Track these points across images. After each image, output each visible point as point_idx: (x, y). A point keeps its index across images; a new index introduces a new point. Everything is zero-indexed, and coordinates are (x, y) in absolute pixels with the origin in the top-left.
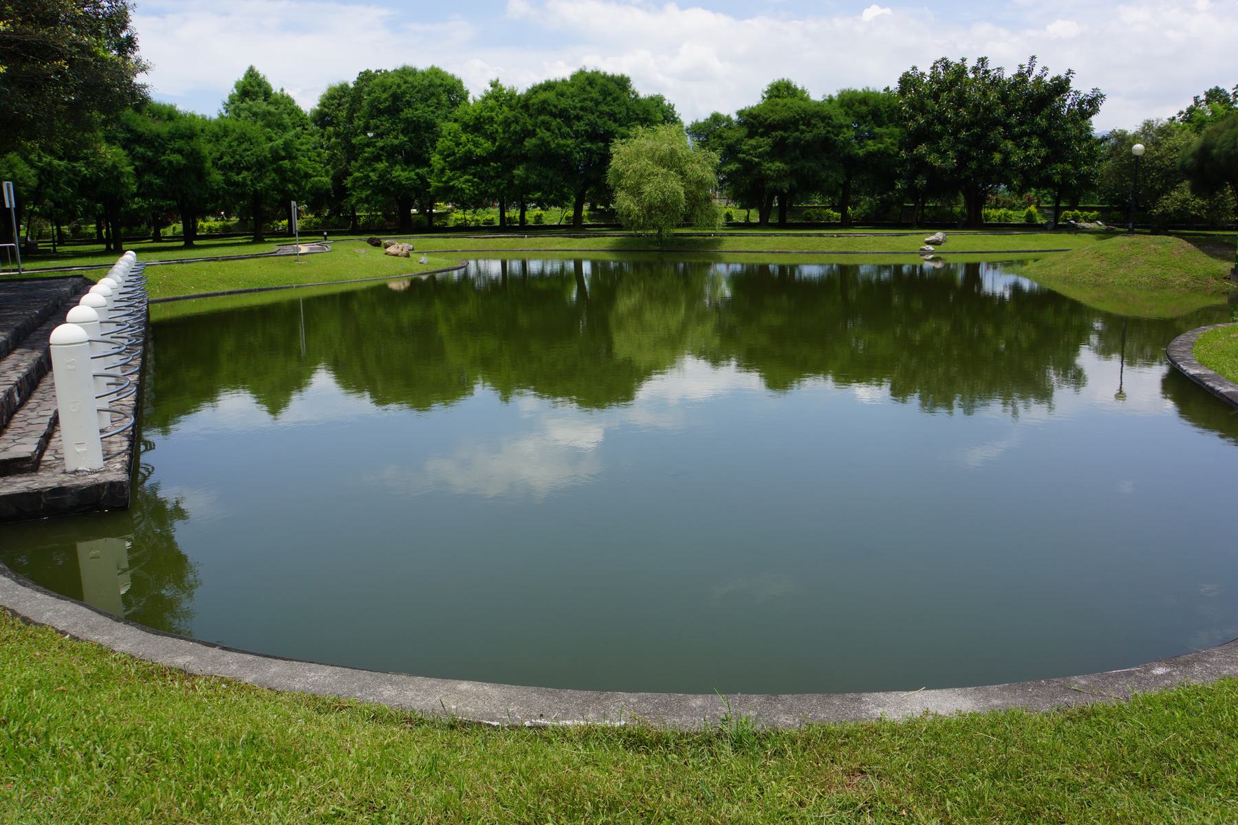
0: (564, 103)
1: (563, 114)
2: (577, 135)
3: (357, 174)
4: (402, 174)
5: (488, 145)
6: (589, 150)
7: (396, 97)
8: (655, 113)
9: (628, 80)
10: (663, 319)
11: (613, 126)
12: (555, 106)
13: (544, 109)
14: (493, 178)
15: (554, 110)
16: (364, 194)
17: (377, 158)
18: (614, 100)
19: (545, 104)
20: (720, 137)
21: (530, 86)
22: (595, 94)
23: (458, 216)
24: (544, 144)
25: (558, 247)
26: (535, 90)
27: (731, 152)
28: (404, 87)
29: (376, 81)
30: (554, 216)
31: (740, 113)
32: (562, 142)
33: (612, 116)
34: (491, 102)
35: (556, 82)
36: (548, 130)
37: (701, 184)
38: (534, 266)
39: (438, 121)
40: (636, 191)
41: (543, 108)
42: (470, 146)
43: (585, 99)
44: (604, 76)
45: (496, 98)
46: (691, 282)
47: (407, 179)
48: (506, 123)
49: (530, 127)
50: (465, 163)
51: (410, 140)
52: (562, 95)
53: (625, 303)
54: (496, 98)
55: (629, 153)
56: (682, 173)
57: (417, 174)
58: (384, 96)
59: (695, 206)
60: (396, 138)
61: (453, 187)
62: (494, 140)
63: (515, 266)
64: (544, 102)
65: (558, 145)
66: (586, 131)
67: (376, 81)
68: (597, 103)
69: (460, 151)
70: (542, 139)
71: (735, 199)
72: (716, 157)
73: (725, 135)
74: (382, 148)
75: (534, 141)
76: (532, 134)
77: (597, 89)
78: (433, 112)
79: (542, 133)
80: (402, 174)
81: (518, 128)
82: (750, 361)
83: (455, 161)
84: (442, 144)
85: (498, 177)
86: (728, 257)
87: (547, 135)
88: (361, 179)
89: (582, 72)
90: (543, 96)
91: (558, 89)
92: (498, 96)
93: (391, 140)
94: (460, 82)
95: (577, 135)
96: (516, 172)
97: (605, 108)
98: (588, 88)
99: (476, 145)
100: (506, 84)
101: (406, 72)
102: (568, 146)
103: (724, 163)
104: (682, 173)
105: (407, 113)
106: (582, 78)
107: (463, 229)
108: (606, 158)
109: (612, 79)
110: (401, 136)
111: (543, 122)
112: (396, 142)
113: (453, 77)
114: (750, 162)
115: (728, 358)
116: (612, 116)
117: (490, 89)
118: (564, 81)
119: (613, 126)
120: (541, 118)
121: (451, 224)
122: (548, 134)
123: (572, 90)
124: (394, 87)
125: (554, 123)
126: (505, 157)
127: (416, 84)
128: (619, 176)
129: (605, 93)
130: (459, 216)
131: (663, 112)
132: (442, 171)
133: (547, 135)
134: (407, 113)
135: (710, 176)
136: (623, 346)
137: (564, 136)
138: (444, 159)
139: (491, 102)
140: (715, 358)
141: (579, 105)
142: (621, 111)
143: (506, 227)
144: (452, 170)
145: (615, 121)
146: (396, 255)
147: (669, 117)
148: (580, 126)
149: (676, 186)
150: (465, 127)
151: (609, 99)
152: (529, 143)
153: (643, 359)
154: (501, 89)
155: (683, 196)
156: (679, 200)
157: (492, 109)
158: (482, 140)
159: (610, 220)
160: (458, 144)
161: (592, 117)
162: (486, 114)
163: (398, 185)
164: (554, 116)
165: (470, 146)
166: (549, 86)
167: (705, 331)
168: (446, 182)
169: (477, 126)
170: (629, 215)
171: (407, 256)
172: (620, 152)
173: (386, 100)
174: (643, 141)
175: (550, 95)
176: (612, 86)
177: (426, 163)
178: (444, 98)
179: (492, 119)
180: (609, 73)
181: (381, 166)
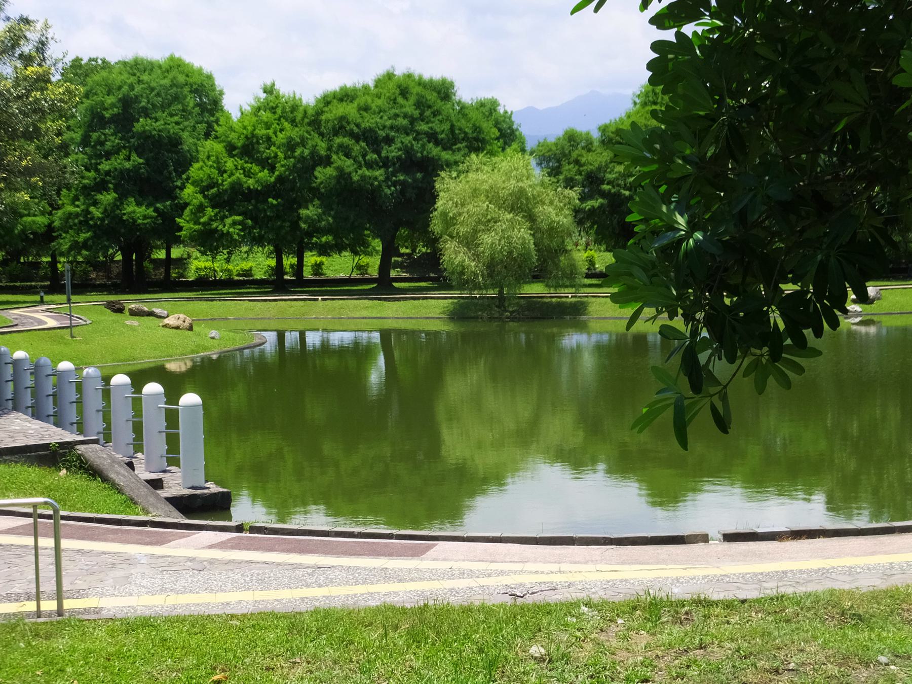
0: (369, 121)
1: (371, 138)
2: (385, 163)
3: (70, 209)
4: (137, 211)
5: (264, 175)
6: (403, 183)
7: (127, 103)
8: (488, 132)
9: (451, 85)
10: (511, 408)
11: (434, 151)
12: (358, 126)
13: (342, 127)
14: (270, 219)
15: (356, 130)
16: (84, 236)
17: (101, 186)
18: (435, 114)
19: (340, 122)
20: (577, 162)
21: (319, 94)
22: (409, 107)
23: (199, 263)
24: (343, 176)
25: (365, 313)
26: (327, 100)
27: (592, 182)
28: (138, 89)
29: (96, 78)
30: (339, 265)
31: (604, 129)
32: (367, 173)
33: (432, 137)
34: (265, 115)
35: (355, 90)
36: (347, 155)
37: (552, 230)
38: (337, 338)
39: (185, 135)
40: (470, 242)
41: (341, 127)
42: (239, 175)
43: (396, 116)
44: (421, 83)
45: (273, 110)
46: (538, 362)
47: (145, 217)
48: (290, 146)
49: (323, 153)
50: (229, 199)
51: (147, 163)
52: (366, 109)
53: (459, 386)
54: (273, 110)
55: (463, 191)
56: (531, 218)
57: (156, 210)
58: (110, 100)
59: (546, 262)
60: (128, 158)
61: (216, 230)
62: (272, 169)
63: (291, 338)
64: (342, 118)
65: (363, 177)
66: (399, 158)
67: (96, 78)
68: (413, 120)
69: (227, 182)
70: (340, 170)
71: (598, 242)
72: (573, 194)
73: (583, 160)
74: (108, 173)
75: (330, 171)
76: (326, 161)
77: (412, 99)
78: (177, 123)
79: (339, 160)
80: (137, 211)
81: (307, 152)
82: (625, 464)
83: (219, 194)
84: (195, 171)
85: (278, 217)
86: (592, 325)
87: (348, 164)
88: (77, 215)
89: (390, 76)
90: (339, 110)
91: (362, 100)
92: (274, 106)
93: (118, 162)
94: (210, 77)
95: (385, 163)
96: (303, 212)
97: (423, 127)
98: (400, 100)
99: (248, 174)
100: (285, 89)
101: (137, 67)
102: (376, 179)
103: (583, 199)
104: (531, 218)
105: (142, 124)
106: (391, 85)
107: (206, 285)
108: (429, 196)
109: (430, 86)
110: (134, 157)
111: (341, 146)
112: (128, 165)
113: (200, 71)
114: (619, 195)
115: (594, 461)
116: (432, 137)
117: (263, 96)
118: (366, 88)
119: (434, 151)
120: (338, 140)
121: (191, 276)
122: (349, 162)
123: (379, 102)
124: (126, 88)
125: (357, 148)
126: (292, 189)
127: (153, 84)
128: (449, 222)
129: (421, 104)
130: (202, 265)
131: (497, 124)
132: (201, 208)
133: (348, 164)
134: (142, 124)
135: (565, 219)
136: (455, 445)
137: (370, 165)
138: (202, 192)
139: (265, 115)
140: (575, 459)
141: (389, 123)
142: (441, 128)
143: (277, 284)
144: (213, 207)
145: (437, 143)
146: (177, 328)
147: (507, 135)
148: (392, 152)
149: (522, 234)
150: (231, 149)
151: (428, 113)
152: (322, 174)
153: (484, 461)
154: (277, 97)
155: (534, 253)
156: (529, 253)
157: (268, 126)
158: (255, 168)
159: (430, 272)
160: (222, 172)
161: (408, 139)
162: (261, 132)
163: (132, 225)
164: (356, 138)
165: (239, 175)
166: (345, 96)
167: (561, 426)
168: (207, 224)
169: (248, 149)
170: (462, 273)
171: (191, 328)
172: (450, 191)
173: (113, 105)
174: (480, 176)
175: (350, 110)
176: (431, 97)
177: (170, 193)
178: (191, 101)
179: (269, 139)
180: (426, 76)
181: (107, 198)
